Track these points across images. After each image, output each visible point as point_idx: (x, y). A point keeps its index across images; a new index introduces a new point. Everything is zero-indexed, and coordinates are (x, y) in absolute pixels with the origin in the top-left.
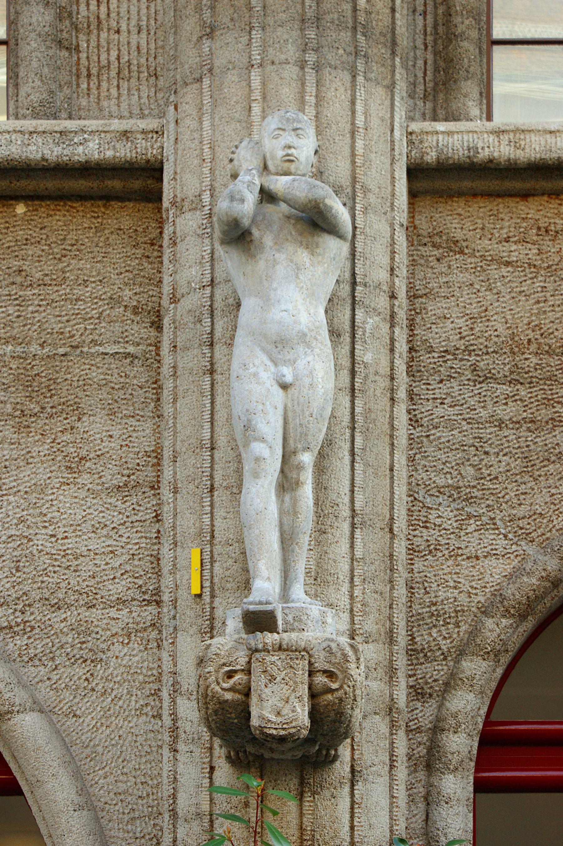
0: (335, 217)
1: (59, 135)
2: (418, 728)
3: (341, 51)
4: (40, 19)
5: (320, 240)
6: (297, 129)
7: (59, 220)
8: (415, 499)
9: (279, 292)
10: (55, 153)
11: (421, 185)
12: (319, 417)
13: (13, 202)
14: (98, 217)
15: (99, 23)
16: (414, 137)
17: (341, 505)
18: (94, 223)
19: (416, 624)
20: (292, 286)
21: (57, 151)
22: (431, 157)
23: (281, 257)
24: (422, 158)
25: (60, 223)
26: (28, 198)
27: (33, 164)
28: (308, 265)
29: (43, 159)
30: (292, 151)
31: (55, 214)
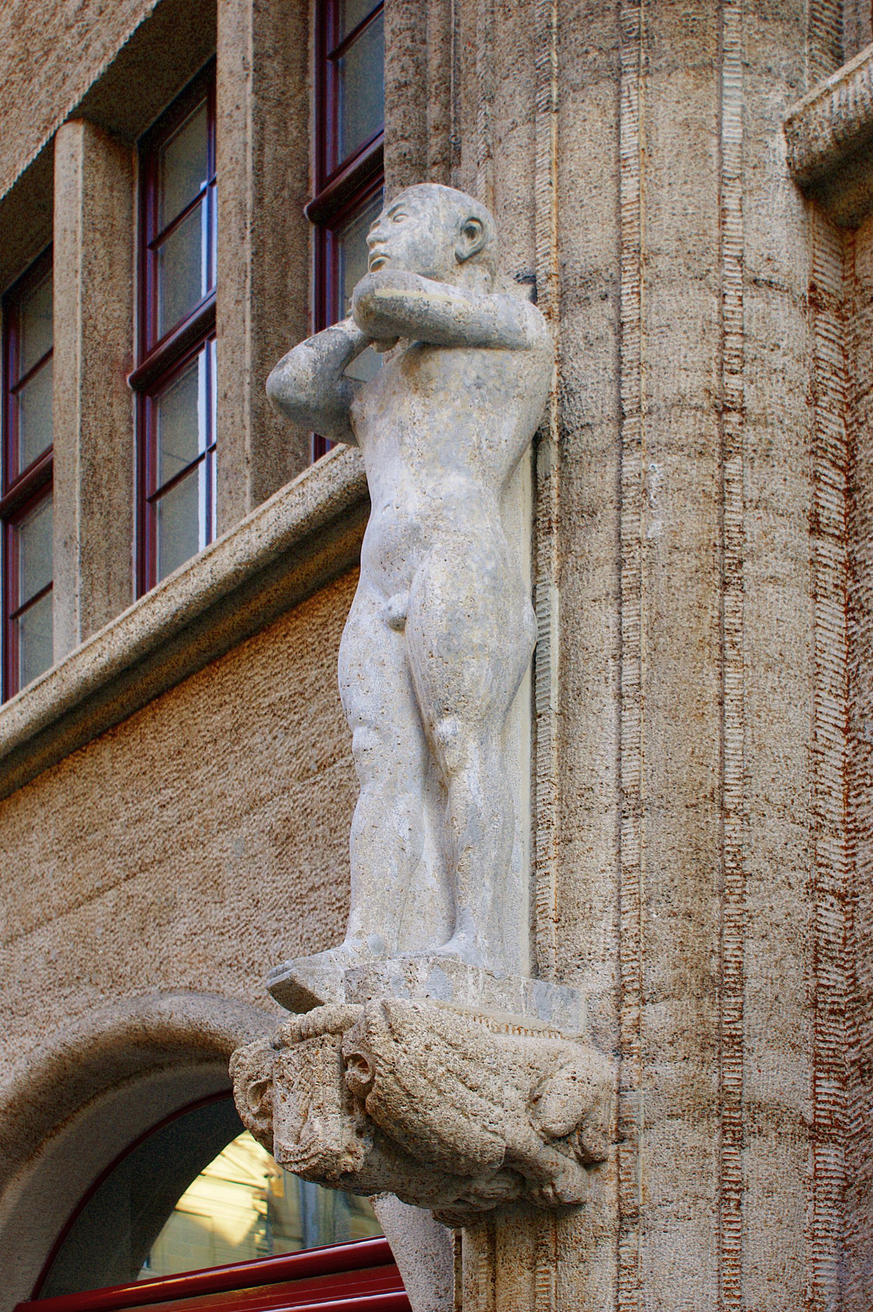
2: (862, 1130)
3: (594, 54)
6: (394, 209)
8: (859, 742)
11: (845, 202)
12: (443, 652)
16: (796, 124)
17: (597, 789)
19: (860, 956)
22: (823, 139)
28: (419, 415)
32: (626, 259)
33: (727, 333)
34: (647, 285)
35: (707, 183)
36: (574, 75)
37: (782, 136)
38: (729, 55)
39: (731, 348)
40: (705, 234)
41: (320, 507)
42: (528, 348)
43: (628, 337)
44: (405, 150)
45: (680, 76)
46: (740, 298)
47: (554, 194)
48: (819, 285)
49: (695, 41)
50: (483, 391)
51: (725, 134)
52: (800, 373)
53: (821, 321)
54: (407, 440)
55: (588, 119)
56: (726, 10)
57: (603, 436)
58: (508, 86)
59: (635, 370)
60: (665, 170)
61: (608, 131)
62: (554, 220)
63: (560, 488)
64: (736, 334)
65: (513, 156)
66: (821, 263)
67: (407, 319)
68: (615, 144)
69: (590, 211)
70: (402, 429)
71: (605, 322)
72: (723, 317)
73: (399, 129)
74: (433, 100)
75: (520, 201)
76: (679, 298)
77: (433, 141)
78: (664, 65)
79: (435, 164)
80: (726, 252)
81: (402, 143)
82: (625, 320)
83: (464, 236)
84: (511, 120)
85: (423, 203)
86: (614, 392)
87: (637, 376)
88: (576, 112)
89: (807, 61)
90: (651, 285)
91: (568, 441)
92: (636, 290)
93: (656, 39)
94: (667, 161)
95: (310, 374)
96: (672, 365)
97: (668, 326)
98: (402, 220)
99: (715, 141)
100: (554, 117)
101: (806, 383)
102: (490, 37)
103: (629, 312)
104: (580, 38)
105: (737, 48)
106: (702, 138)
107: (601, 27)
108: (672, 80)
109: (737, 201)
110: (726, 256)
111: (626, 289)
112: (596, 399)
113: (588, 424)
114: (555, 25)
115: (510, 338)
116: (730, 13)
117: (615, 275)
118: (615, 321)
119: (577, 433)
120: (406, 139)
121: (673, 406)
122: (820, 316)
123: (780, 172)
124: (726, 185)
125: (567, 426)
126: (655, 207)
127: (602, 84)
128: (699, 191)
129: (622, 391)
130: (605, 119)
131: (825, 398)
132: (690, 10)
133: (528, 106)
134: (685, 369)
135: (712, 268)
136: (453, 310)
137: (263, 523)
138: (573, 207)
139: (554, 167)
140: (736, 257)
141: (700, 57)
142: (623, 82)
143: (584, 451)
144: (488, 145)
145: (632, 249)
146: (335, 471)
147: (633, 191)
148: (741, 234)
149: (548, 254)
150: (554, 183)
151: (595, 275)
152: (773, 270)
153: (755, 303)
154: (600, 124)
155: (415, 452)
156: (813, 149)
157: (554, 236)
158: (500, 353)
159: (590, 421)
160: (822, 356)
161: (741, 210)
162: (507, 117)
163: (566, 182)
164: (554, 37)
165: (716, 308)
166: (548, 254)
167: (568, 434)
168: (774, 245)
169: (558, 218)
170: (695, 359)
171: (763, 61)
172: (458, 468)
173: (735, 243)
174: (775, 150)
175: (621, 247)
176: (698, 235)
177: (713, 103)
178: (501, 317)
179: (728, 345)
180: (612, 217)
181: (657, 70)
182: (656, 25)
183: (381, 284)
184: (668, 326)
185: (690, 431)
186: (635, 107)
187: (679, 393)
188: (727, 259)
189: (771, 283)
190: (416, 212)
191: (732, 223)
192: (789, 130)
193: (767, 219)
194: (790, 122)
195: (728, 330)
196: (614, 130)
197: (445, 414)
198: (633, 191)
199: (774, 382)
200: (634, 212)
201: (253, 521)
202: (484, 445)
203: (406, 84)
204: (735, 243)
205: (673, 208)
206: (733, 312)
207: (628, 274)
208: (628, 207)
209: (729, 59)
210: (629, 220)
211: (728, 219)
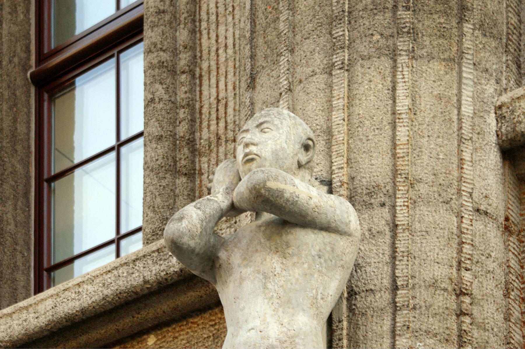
0: (295, 203)
1: (157, 253)
3: (377, 37)
4: (153, 155)
5: (291, 237)
6: (261, 124)
7: (183, 339)
9: (246, 311)
10: (154, 272)
13: (145, 337)
14: (215, 324)
15: (219, 138)
16: (504, 109)
18: (211, 332)
20: (260, 299)
21: (155, 269)
23: (248, 271)
24: (514, 130)
25: (184, 342)
26: (158, 326)
27: (139, 290)
28: (278, 270)
29: (146, 282)
30: (253, 149)
31: (180, 335)
32: (400, 182)
33: (463, 243)
34: (412, 201)
35: (451, 140)
36: (362, 48)
37: (494, 115)
38: (466, 56)
39: (466, 253)
40: (449, 174)
41: (94, 304)
42: (350, 235)
43: (401, 235)
44: (163, 59)
45: (436, 63)
46: (471, 220)
47: (345, 127)
48: (511, 218)
49: (445, 42)
50: (322, 260)
51: (463, 109)
52: (499, 273)
53: (511, 242)
54: (269, 286)
55: (372, 80)
56: (464, 25)
57: (382, 299)
58: (308, 45)
59: (406, 258)
60: (425, 126)
61: (386, 92)
62: (346, 145)
63: (349, 328)
64: (469, 244)
65: (312, 95)
66: (511, 203)
67: (284, 205)
68: (391, 102)
69: (373, 145)
70: (266, 278)
71: (384, 222)
72: (461, 232)
73: (158, 43)
74: (182, 26)
75: (318, 127)
76: (434, 214)
77: (182, 56)
78: (425, 54)
79: (183, 72)
80: (463, 188)
81: (162, 53)
82: (399, 223)
83: (303, 150)
84: (311, 69)
85: (281, 123)
86: (389, 270)
87: (407, 263)
88: (364, 74)
89: (504, 67)
90: (415, 202)
91: (356, 299)
92: (406, 204)
93: (420, 35)
94: (427, 120)
95: (199, 228)
96: (429, 258)
97: (427, 232)
98: (268, 132)
99: (456, 112)
100: (346, 74)
101: (503, 282)
102: (291, 7)
103: (402, 218)
104: (367, 23)
105: (471, 52)
106: (449, 108)
107: (383, 19)
108: (431, 66)
109: (470, 155)
110: (463, 191)
111: (399, 202)
112: (378, 274)
113: (371, 290)
114: (347, 11)
115: (342, 227)
116: (467, 27)
117: (390, 191)
118: (390, 222)
119: (363, 294)
120: (164, 51)
121: (430, 286)
122: (511, 239)
123: (492, 139)
124: (464, 143)
125: (355, 288)
126: (418, 150)
127: (382, 58)
128: (447, 145)
129: (397, 271)
130: (385, 84)
131: (513, 293)
132: (442, 21)
133: (325, 62)
134: (438, 263)
135: (454, 197)
136: (312, 203)
137: (41, 308)
138: (361, 140)
139: (346, 108)
140: (469, 193)
141: (448, 53)
142: (399, 61)
143: (369, 308)
144: (290, 82)
145: (404, 176)
146: (109, 280)
147: (404, 136)
148: (472, 178)
149: (342, 168)
150: (346, 119)
151: (376, 188)
152: (488, 204)
153: (479, 226)
154: (381, 86)
155: (275, 295)
156: (517, 129)
157: (345, 156)
158: (333, 236)
159: (373, 288)
160: (512, 265)
161: (472, 162)
162: (308, 66)
163: (355, 121)
164: (346, 18)
165: (456, 224)
166: (342, 168)
167: (356, 294)
168: (489, 188)
169: (348, 144)
170: (444, 257)
171: (484, 63)
172: (303, 310)
173: (469, 183)
174: (490, 124)
175: (395, 173)
176: (445, 173)
177: (455, 86)
178: (338, 212)
179: (464, 250)
180: (389, 151)
181: (420, 57)
182: (420, 26)
183: (271, 179)
184: (427, 232)
185: (440, 304)
186: (407, 80)
187: (434, 278)
188: (464, 193)
189: (487, 213)
190: (278, 129)
191: (467, 169)
192: (499, 112)
193: (485, 170)
194: (500, 107)
195: (464, 240)
196: (390, 92)
197: (297, 272)
198: (404, 136)
199: (488, 279)
200: (405, 150)
201: (31, 305)
202: (319, 297)
203: (164, 12)
204: (469, 183)
205: (431, 153)
206: (467, 229)
207: (401, 192)
208: (402, 147)
209: (466, 58)
210: (402, 155)
211: (465, 166)
